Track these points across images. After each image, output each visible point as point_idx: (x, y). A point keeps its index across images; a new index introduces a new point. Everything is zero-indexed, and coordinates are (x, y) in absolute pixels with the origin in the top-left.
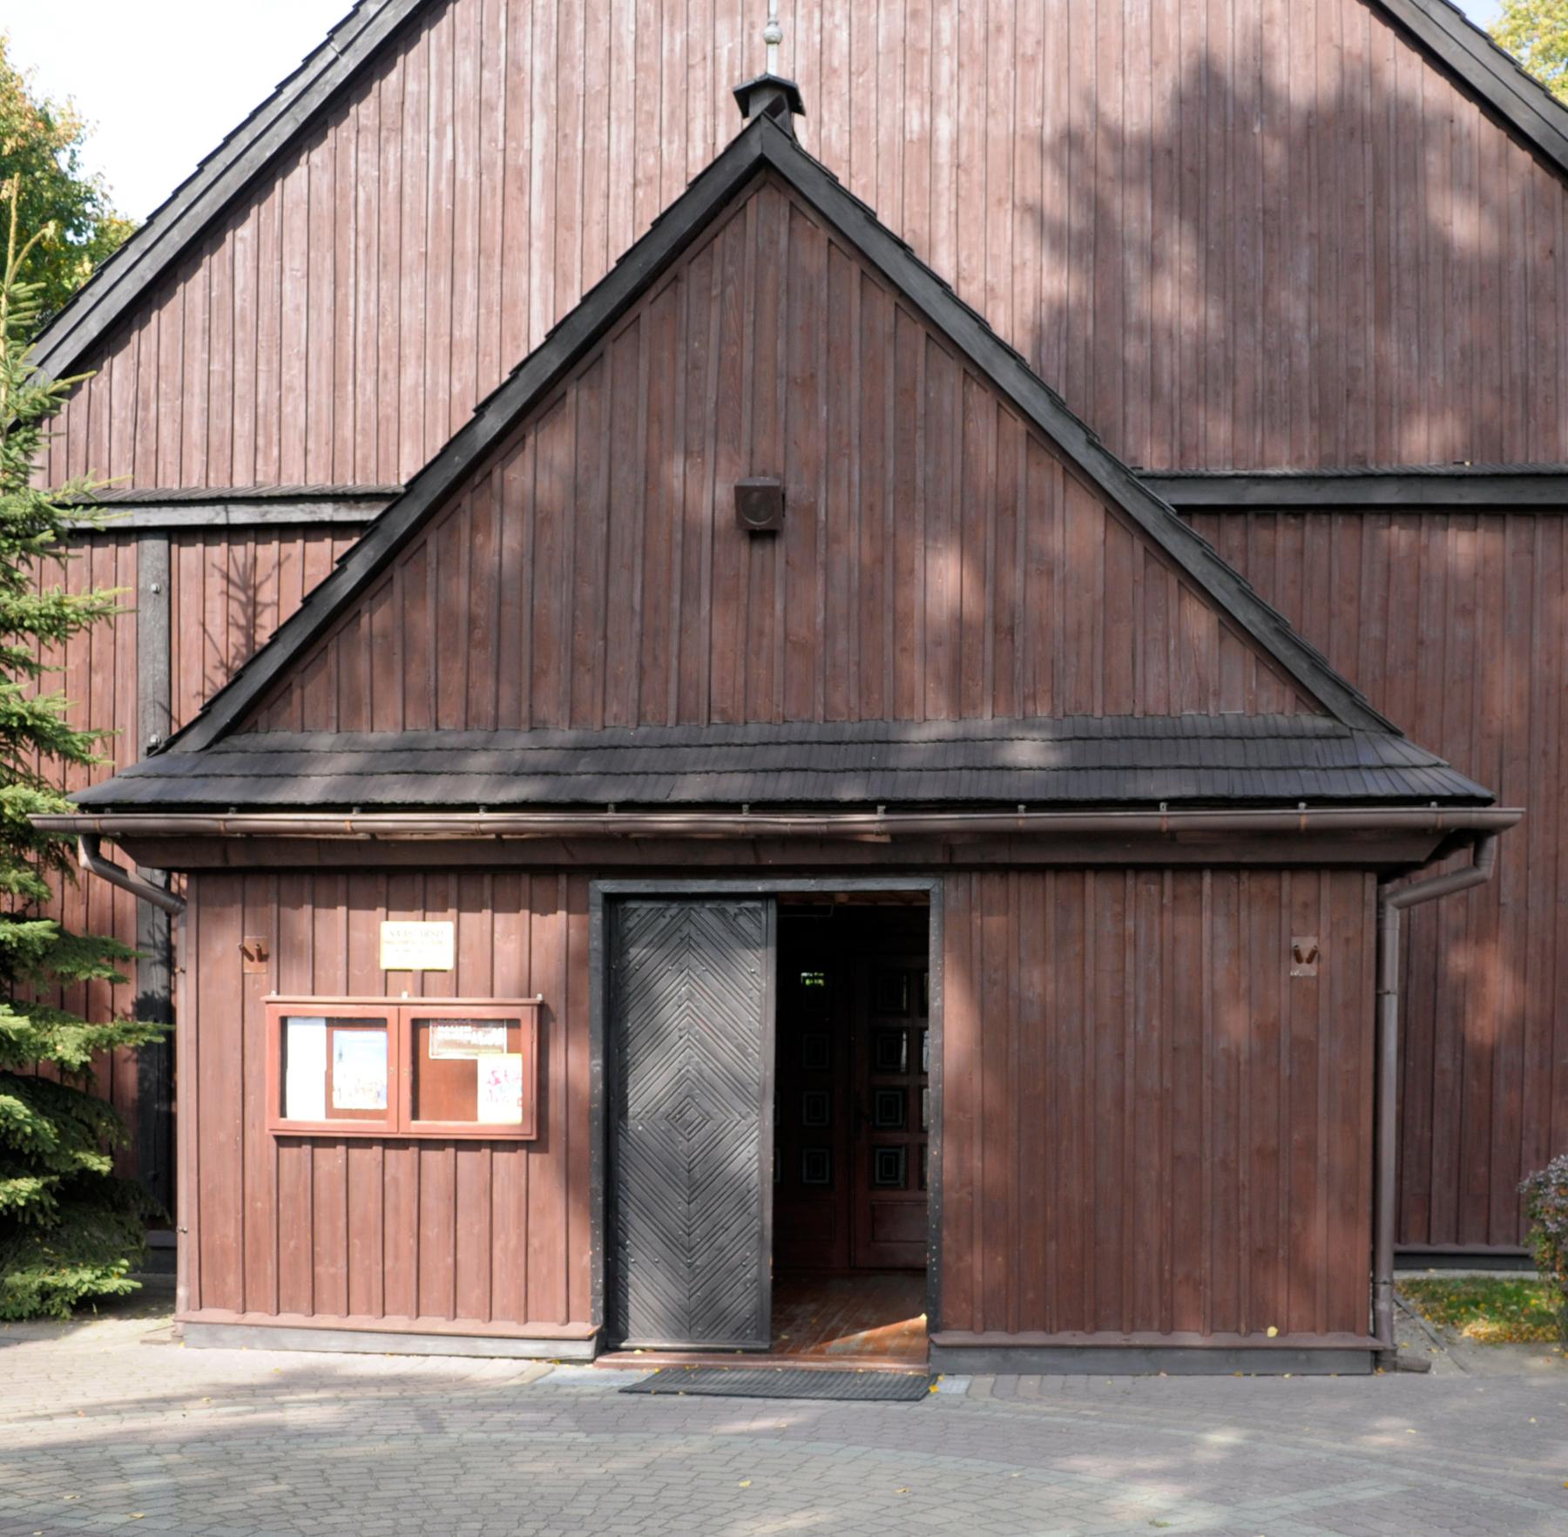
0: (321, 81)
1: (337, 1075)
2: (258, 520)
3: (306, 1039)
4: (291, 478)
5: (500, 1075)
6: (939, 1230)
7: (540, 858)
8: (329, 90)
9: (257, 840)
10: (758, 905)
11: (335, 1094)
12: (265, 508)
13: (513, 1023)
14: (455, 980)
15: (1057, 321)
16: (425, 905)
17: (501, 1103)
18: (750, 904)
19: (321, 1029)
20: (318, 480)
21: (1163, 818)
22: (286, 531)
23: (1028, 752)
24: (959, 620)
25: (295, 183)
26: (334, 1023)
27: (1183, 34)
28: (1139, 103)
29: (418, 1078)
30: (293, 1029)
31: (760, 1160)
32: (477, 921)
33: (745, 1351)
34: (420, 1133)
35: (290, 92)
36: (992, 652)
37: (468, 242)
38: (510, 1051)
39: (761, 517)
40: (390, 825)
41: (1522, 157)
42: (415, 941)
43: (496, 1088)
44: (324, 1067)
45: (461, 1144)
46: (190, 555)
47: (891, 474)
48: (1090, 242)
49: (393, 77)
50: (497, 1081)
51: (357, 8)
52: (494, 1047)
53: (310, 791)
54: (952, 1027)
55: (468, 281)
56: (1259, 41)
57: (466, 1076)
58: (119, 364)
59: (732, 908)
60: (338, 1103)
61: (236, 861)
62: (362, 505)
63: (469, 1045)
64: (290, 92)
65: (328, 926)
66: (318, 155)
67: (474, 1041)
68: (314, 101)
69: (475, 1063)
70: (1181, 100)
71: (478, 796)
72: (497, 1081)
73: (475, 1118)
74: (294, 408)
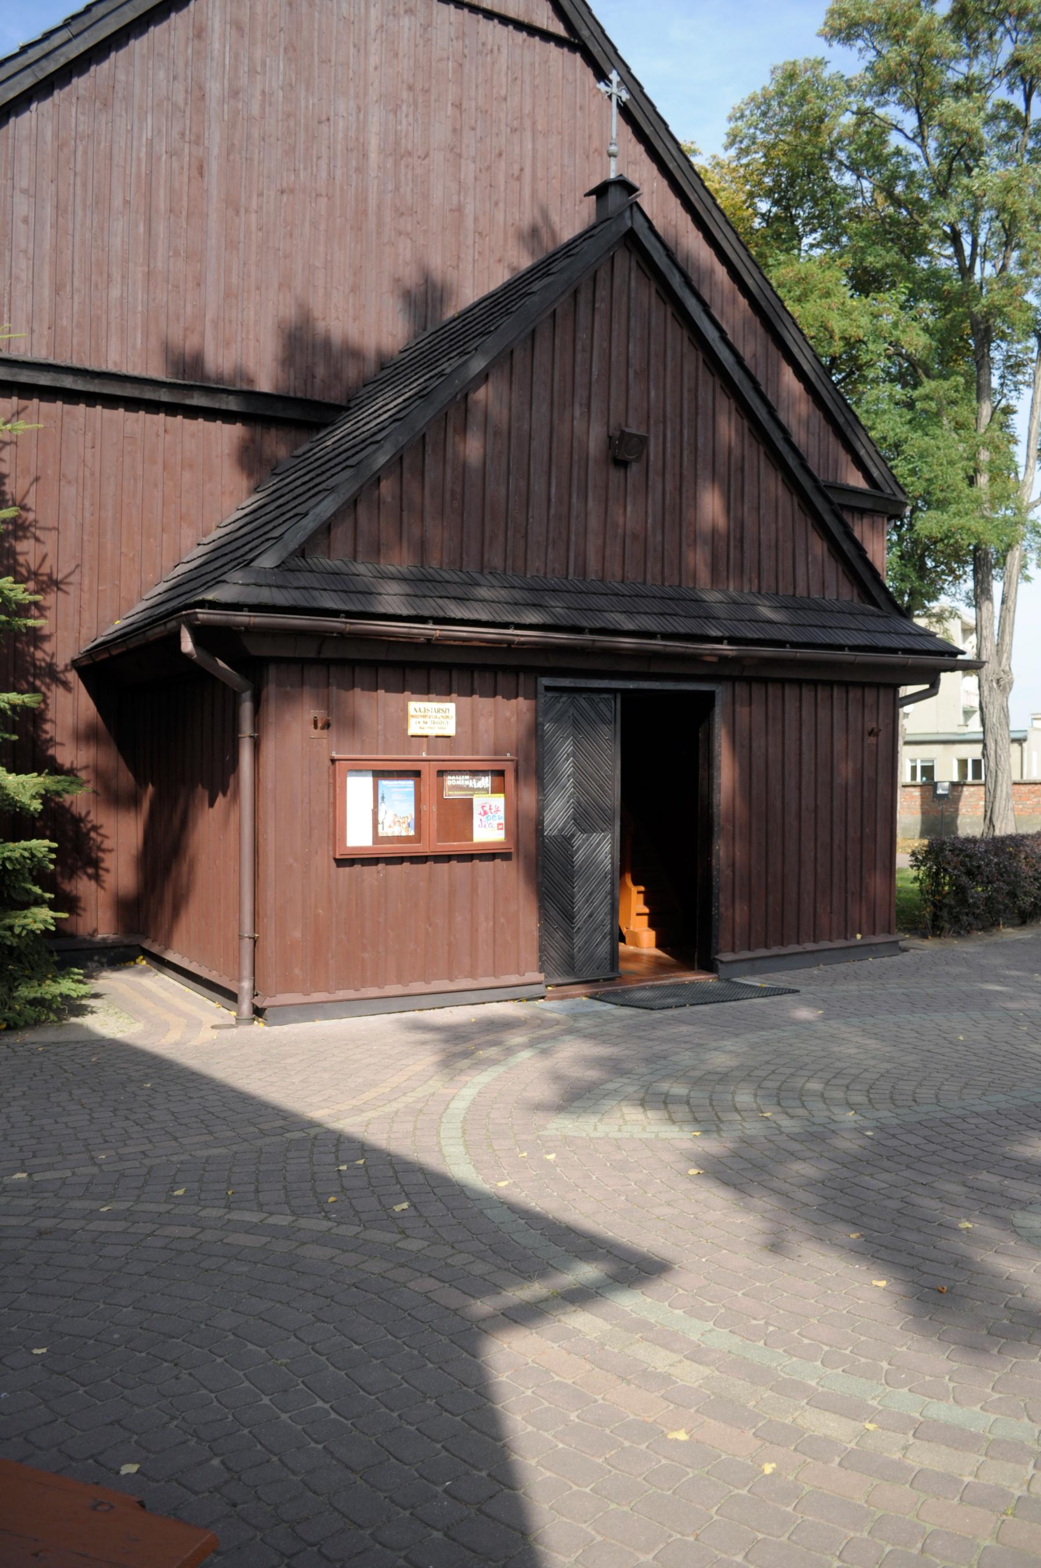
0: (58, 52)
1: (374, 811)
2: (10, 378)
3: (358, 788)
4: (18, 349)
5: (487, 809)
6: (718, 894)
7: (491, 660)
8: (63, 61)
9: (435, 645)
10: (610, 696)
11: (380, 827)
12: (16, 370)
13: (501, 773)
16: (445, 691)
17: (489, 827)
18: (606, 696)
19: (368, 780)
21: (846, 655)
24: (714, 530)
26: (379, 774)
30: (409, 784)
31: (612, 858)
32: (483, 704)
33: (605, 980)
34: (436, 852)
35: (34, 54)
36: (731, 551)
37: (161, 201)
38: (493, 792)
39: (623, 451)
40: (465, 634)
41: (743, 302)
42: (432, 717)
43: (484, 818)
44: (371, 807)
45: (469, 857)
49: (105, 65)
50: (485, 813)
51: (88, 9)
52: (483, 789)
54: (726, 774)
55: (161, 228)
59: (596, 697)
60: (382, 832)
61: (328, 653)
62: (96, 381)
63: (468, 788)
64: (34, 54)
65: (371, 705)
66: (46, 105)
67: (471, 785)
68: (51, 66)
69: (472, 800)
72: (485, 813)
73: (471, 839)
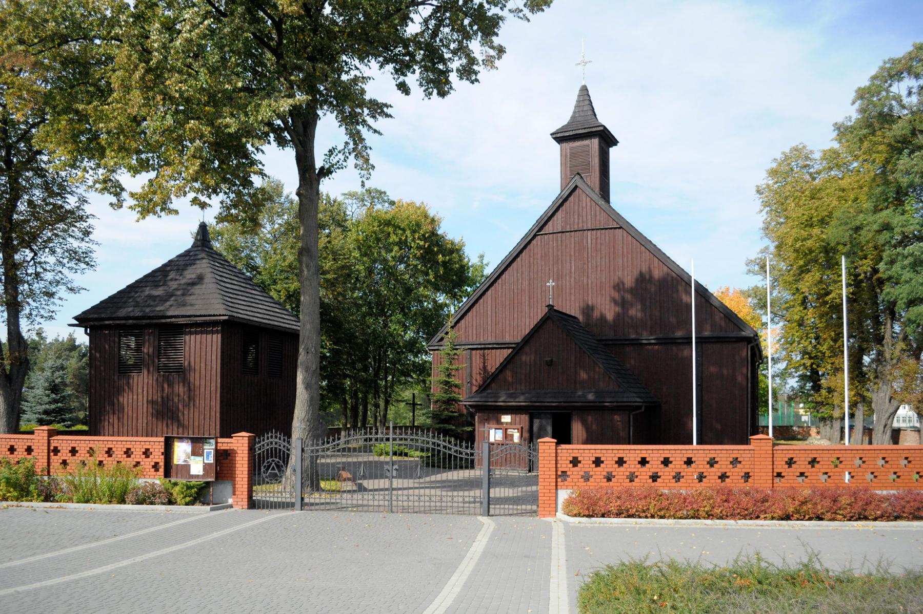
1: (495, 435)
14: (511, 423)
15: (617, 316)
16: (507, 414)
20: (493, 341)
22: (489, 349)
23: (591, 397)
25: (489, 292)
27: (856, 88)
28: (629, 281)
29: (506, 435)
42: (506, 419)
46: (474, 352)
47: (328, 461)
48: (623, 304)
53: (501, 400)
56: (650, 268)
57: (512, 436)
58: (463, 321)
70: (637, 280)
71: (521, 401)
74: (489, 328)
